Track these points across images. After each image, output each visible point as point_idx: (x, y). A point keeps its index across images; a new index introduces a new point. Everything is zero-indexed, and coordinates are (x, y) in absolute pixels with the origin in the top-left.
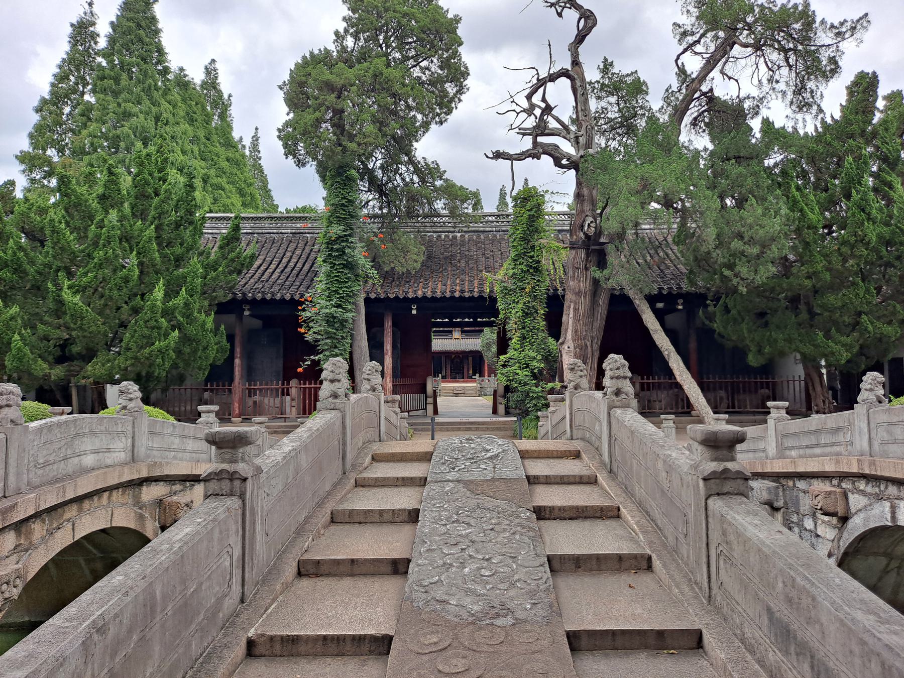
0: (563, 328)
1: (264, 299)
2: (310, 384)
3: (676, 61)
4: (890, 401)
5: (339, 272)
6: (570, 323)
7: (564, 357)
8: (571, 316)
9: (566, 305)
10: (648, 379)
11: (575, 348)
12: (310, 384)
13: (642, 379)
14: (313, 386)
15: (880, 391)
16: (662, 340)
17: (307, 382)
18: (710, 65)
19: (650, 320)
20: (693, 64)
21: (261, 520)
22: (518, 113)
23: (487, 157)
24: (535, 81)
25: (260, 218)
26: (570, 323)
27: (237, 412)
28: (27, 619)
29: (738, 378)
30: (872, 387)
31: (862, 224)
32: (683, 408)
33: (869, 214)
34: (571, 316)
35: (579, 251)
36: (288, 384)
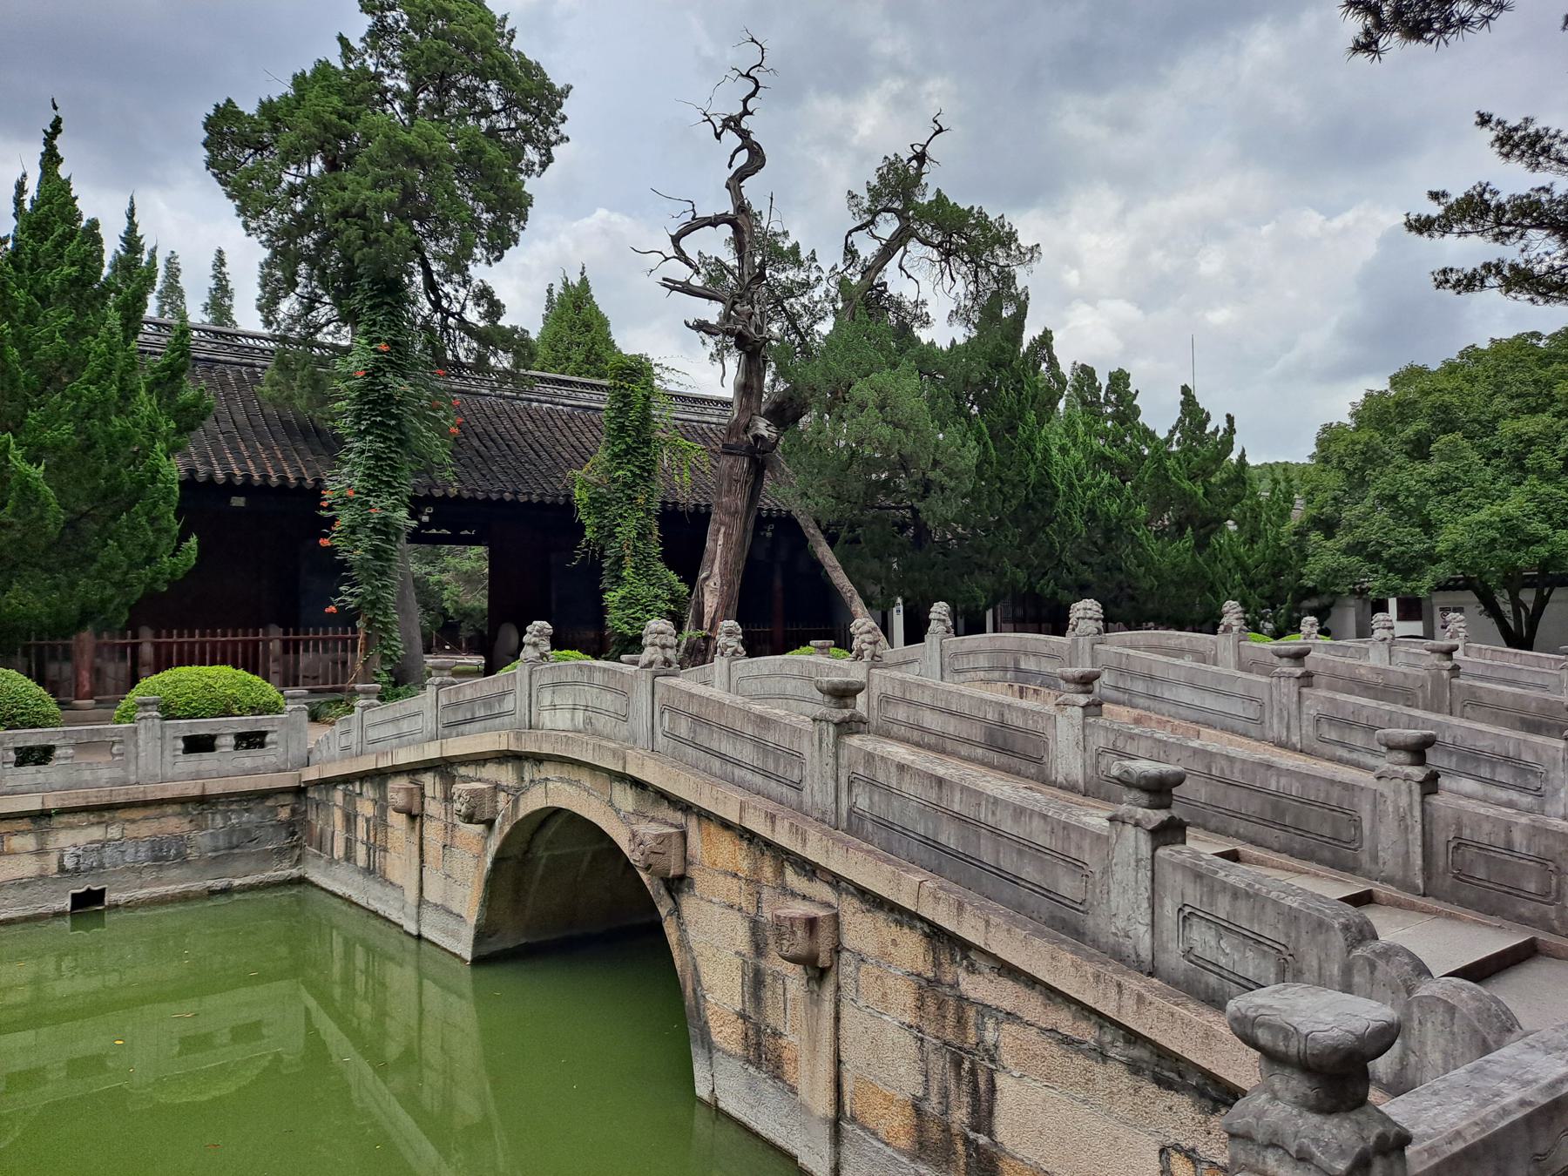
0: (706, 556)
1: (541, 503)
2: (180, 635)
3: (850, 233)
4: (698, 653)
5: (392, 452)
6: (719, 551)
7: (706, 596)
8: (720, 542)
9: (711, 527)
10: (245, 634)
11: (722, 585)
12: (180, 635)
13: (286, 633)
14: (240, 638)
15: (546, 646)
16: (840, 579)
17: (251, 630)
18: (887, 252)
19: (826, 554)
20: (867, 248)
21: (1213, 712)
22: (667, 259)
23: (688, 325)
24: (688, 218)
25: (569, 383)
26: (719, 551)
27: (87, 688)
28: (523, 941)
29: (245, 634)
30: (537, 639)
31: (1028, 465)
32: (335, 682)
33: (1033, 455)
34: (720, 542)
35: (741, 458)
36: (135, 636)
